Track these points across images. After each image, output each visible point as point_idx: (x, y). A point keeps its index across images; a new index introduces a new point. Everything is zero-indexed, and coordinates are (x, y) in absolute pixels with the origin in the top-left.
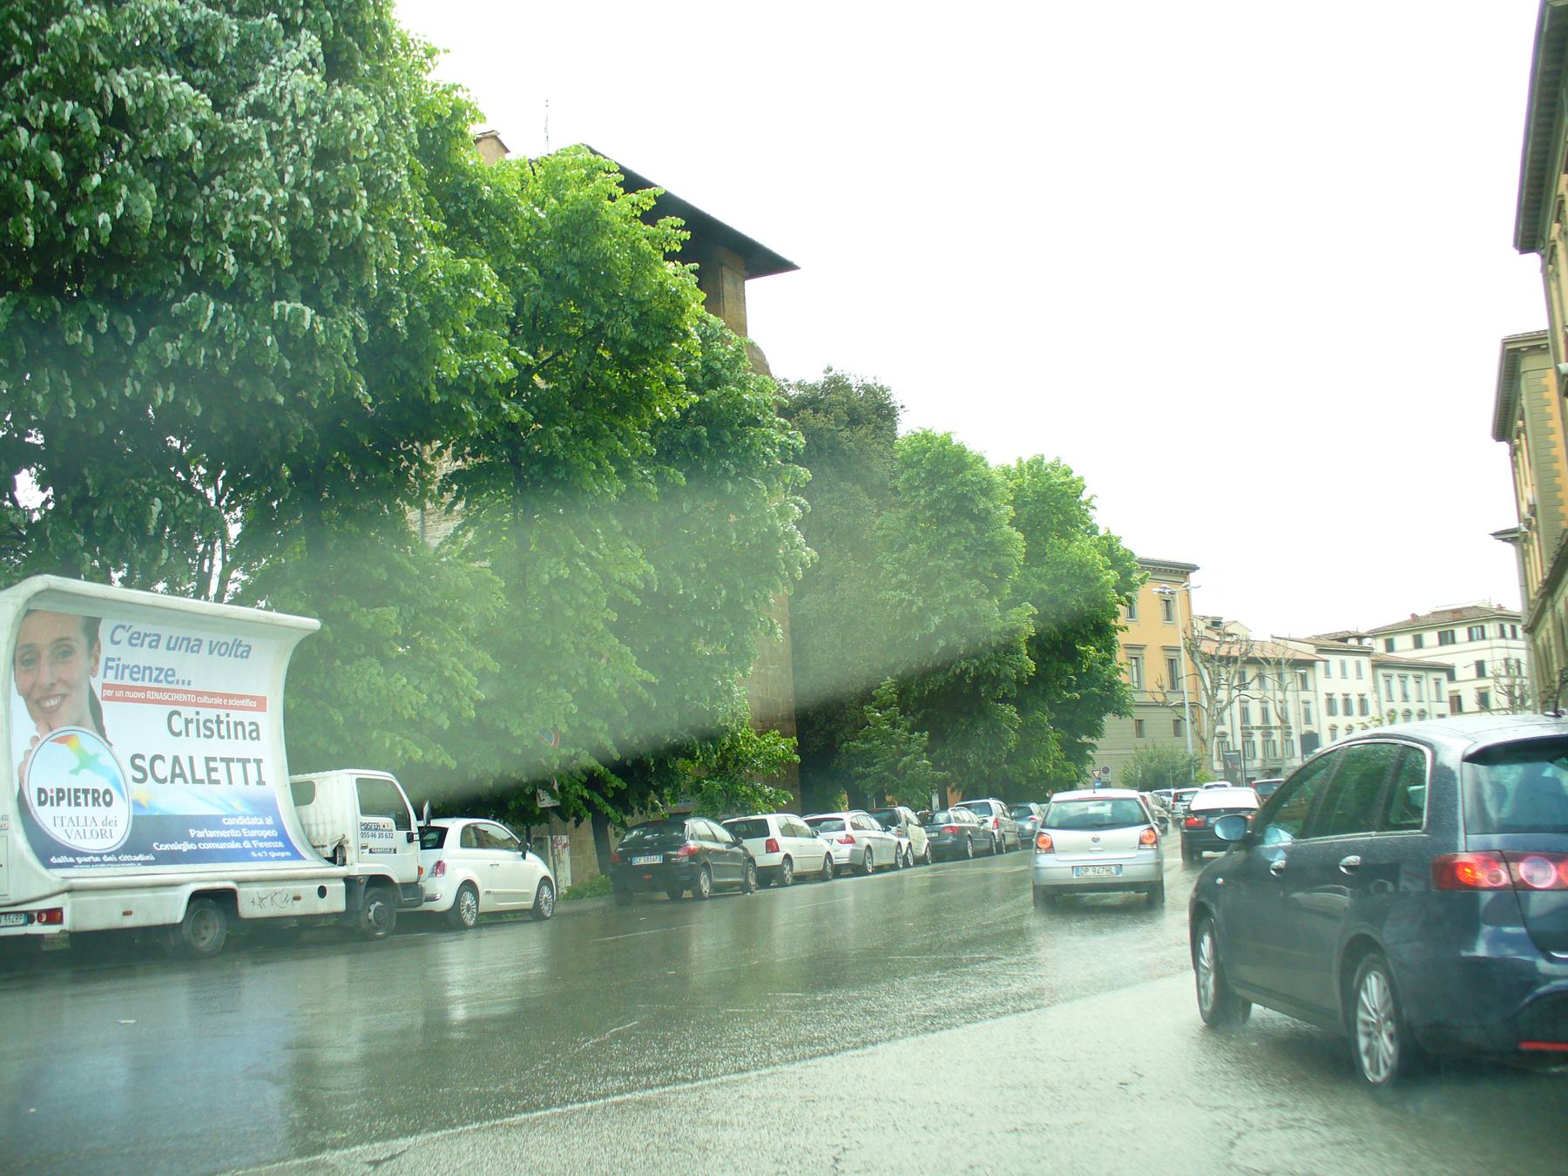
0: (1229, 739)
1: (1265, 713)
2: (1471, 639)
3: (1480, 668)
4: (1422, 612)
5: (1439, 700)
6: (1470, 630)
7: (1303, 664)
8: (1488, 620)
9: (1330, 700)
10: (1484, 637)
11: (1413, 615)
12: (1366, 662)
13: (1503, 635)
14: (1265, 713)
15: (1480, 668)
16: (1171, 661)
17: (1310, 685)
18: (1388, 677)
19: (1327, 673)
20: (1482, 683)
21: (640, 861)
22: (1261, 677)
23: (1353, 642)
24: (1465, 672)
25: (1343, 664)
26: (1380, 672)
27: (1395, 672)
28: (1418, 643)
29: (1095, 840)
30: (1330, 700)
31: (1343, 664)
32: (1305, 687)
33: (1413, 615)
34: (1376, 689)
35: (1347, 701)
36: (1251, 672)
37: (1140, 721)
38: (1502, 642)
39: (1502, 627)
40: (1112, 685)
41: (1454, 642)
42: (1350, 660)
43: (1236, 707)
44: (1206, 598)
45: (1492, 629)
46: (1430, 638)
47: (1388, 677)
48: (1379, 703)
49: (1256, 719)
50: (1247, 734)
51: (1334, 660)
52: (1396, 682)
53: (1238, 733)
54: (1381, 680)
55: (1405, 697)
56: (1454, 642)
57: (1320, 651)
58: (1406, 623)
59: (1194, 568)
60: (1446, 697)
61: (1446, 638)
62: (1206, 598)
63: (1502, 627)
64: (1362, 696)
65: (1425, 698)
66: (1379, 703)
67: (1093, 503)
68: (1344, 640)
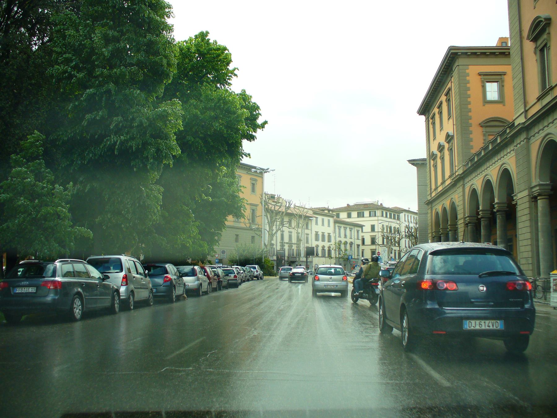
0: (275, 247)
1: (290, 237)
2: (370, 216)
3: (373, 227)
4: (351, 204)
5: (358, 239)
6: (370, 213)
7: (307, 218)
8: (378, 209)
10: (375, 216)
11: (348, 205)
12: (332, 220)
13: (382, 216)
14: (290, 237)
15: (373, 227)
16: (253, 210)
17: (309, 228)
18: (340, 227)
19: (317, 223)
22: (290, 222)
23: (326, 211)
24: (367, 228)
25: (323, 220)
26: (337, 225)
27: (343, 226)
28: (349, 216)
29: (331, 278)
31: (323, 220)
32: (307, 228)
33: (348, 205)
34: (335, 232)
35: (323, 235)
36: (286, 219)
37: (237, 235)
38: (382, 218)
39: (382, 212)
40: (234, 197)
41: (363, 216)
42: (326, 219)
43: (279, 233)
44: (270, 185)
45: (378, 213)
46: (354, 214)
47: (340, 227)
48: (335, 238)
49: (286, 239)
50: (282, 245)
51: (320, 218)
52: (342, 230)
53: (279, 244)
54: (337, 228)
56: (363, 216)
57: (315, 213)
58: (345, 207)
60: (360, 238)
61: (361, 215)
62: (270, 185)
63: (382, 212)
64: (329, 234)
65: (353, 237)
66: (335, 238)
67: (236, 72)
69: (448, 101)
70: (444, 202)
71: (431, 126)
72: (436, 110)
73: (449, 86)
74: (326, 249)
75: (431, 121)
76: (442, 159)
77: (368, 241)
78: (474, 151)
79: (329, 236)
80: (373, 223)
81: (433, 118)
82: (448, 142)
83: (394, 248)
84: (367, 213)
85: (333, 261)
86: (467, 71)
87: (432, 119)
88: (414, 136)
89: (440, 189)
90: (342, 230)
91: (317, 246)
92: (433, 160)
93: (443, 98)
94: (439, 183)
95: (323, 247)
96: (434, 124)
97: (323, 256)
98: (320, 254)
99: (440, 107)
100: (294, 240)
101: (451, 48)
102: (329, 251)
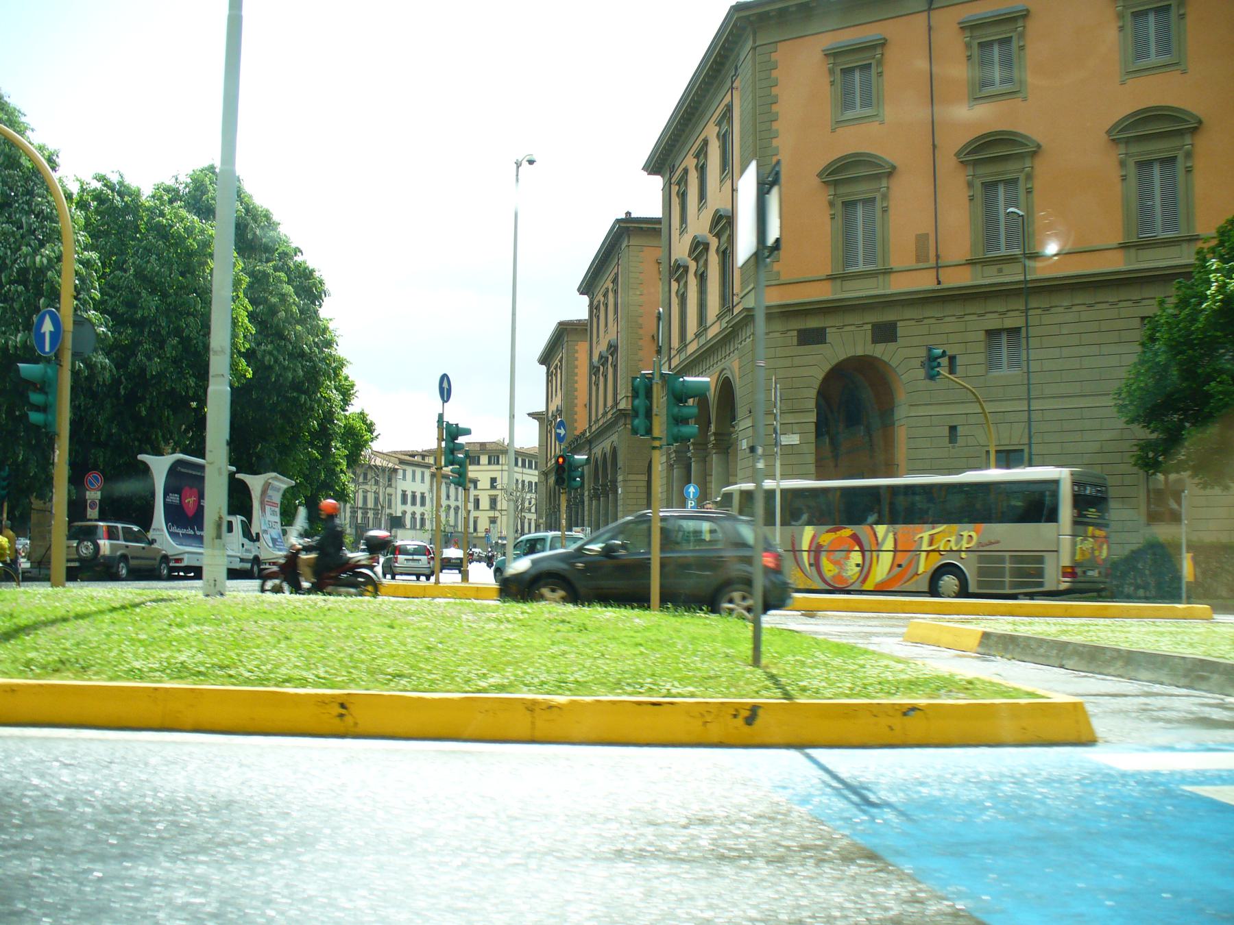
1: (365, 499)
3: (493, 480)
9: (404, 495)
12: (427, 473)
14: (365, 499)
20: (493, 492)
21: (1164, 895)
30: (404, 495)
32: (390, 486)
35: (414, 497)
41: (479, 464)
42: (418, 471)
51: (409, 470)
52: (444, 487)
55: (448, 497)
56: (479, 464)
57: (402, 462)
59: (1025, 15)
68: (413, 456)
69: (724, 139)
70: (603, 444)
71: (676, 201)
72: (690, 162)
73: (727, 99)
74: (418, 517)
75: (675, 189)
76: (702, 278)
77: (485, 503)
78: (577, 433)
79: (423, 497)
80: (494, 475)
81: (683, 180)
82: (696, 259)
83: (528, 516)
84: (484, 459)
85: (428, 536)
86: (774, 57)
87: (679, 184)
88: (534, 391)
89: (692, 348)
90: (444, 487)
91: (404, 513)
92: (678, 280)
93: (711, 131)
94: (690, 334)
95: (414, 514)
96: (683, 196)
97: (413, 527)
98: (408, 526)
99: (702, 152)
100: (370, 504)
101: (561, 324)
102: (423, 520)
